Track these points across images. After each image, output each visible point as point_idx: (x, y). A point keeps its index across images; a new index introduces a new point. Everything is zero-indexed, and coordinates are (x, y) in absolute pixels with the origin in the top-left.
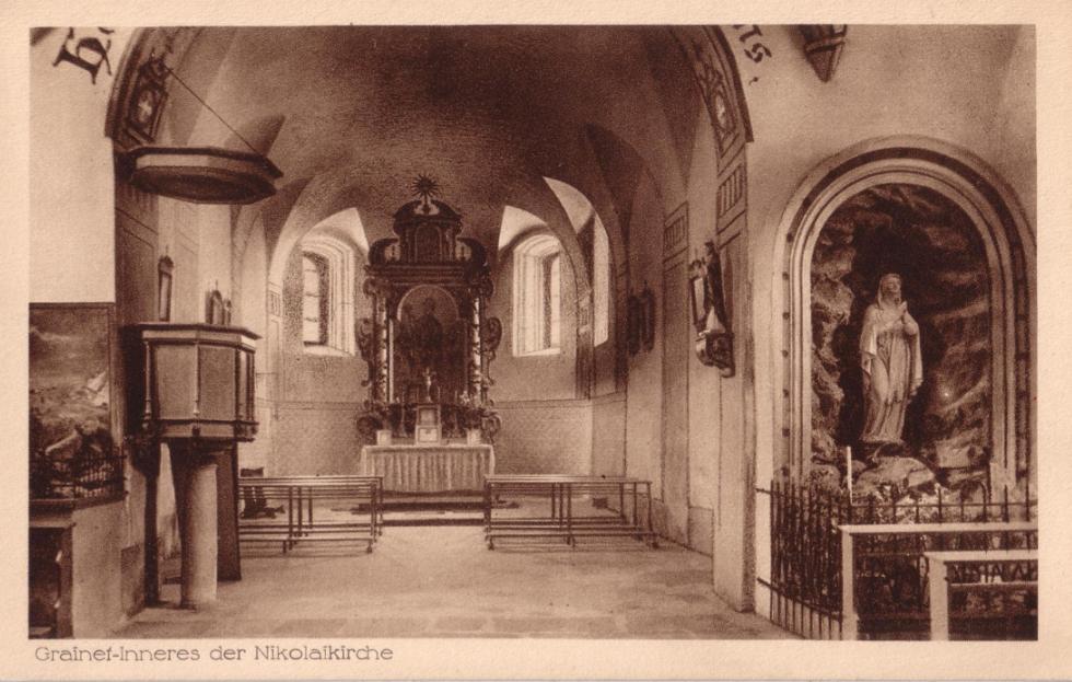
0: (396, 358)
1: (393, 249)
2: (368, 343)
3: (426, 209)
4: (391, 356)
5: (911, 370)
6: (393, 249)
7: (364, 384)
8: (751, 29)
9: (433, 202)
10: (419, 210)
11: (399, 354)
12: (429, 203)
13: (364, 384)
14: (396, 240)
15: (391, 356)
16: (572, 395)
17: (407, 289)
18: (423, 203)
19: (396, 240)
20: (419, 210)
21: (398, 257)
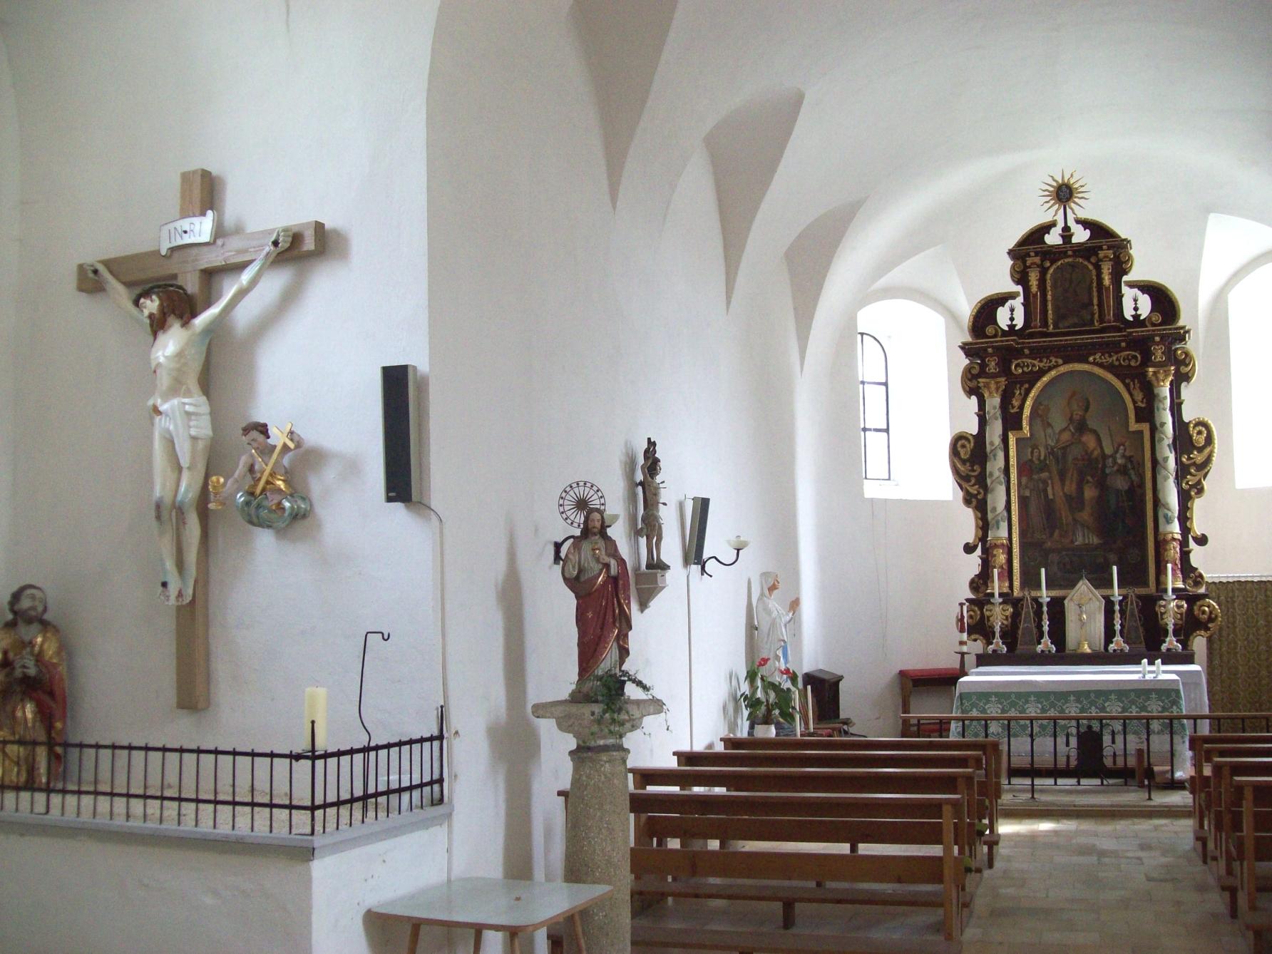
0: (1023, 501)
1: (1012, 310)
2: (969, 458)
3: (1067, 233)
4: (1013, 461)
5: (900, 903)
6: (1012, 310)
7: (969, 549)
8: (1199, 843)
9: (1078, 221)
10: (1053, 238)
11: (1027, 493)
12: (1071, 223)
13: (969, 549)
14: (1012, 296)
15: (1013, 461)
16: (457, 871)
17: (1042, 373)
18: (1061, 225)
19: (1012, 296)
20: (1053, 238)
21: (1019, 322)
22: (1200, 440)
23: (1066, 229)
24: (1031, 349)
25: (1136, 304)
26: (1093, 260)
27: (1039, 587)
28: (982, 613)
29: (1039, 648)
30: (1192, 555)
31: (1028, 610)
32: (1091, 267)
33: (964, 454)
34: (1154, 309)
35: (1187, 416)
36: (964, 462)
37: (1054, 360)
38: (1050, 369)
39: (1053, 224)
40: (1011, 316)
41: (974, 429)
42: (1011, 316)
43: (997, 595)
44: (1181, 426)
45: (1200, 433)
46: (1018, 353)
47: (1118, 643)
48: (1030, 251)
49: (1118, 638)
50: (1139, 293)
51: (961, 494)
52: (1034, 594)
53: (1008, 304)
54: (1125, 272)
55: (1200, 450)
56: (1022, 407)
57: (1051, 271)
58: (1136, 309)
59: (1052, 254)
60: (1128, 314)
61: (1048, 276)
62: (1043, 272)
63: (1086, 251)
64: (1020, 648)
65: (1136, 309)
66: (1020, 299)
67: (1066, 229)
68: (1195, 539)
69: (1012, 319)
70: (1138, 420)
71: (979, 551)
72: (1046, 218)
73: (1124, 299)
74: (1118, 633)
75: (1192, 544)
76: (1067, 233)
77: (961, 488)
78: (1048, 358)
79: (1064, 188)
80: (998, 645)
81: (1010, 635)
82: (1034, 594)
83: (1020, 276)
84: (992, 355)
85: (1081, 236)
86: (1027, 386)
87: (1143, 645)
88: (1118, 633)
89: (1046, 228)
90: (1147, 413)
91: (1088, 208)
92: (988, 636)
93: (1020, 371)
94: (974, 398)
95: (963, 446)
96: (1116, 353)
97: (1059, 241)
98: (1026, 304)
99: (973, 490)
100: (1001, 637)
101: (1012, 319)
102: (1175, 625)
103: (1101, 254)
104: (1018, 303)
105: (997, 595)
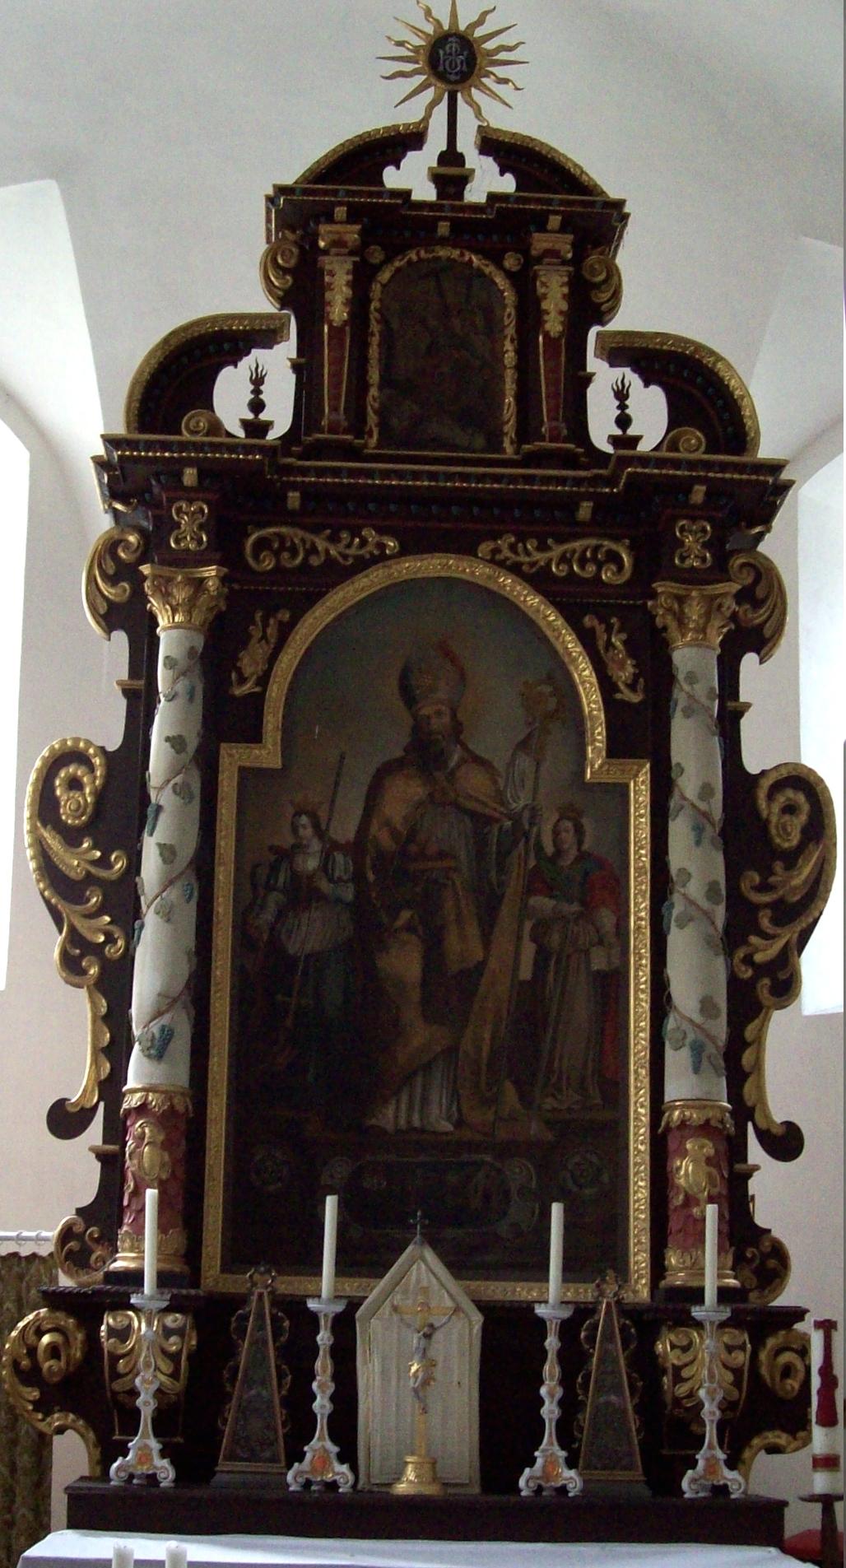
1: (258, 381)
3: (451, 174)
6: (258, 381)
7: (65, 1121)
10: (412, 176)
12: (467, 143)
14: (262, 334)
17: (338, 573)
20: (412, 176)
21: (280, 415)
22: (787, 834)
23: (451, 157)
24: (307, 493)
25: (626, 412)
26: (511, 262)
27: (540, 1270)
28: (93, 1340)
29: (293, 1478)
30: (754, 1186)
31: (256, 1345)
32: (500, 281)
33: (71, 806)
34: (676, 419)
35: (754, 760)
36: (72, 837)
37: (370, 534)
38: (362, 565)
39: (414, 138)
40: (262, 392)
41: (113, 736)
42: (262, 392)
43: (710, 1295)
44: (738, 782)
45: (790, 809)
46: (270, 507)
47: (550, 1467)
48: (337, 210)
49: (549, 1449)
50: (634, 380)
51: (56, 941)
52: (288, 1285)
53: (247, 363)
54: (600, 316)
55: (791, 859)
56: (264, 680)
57: (385, 275)
58: (623, 421)
59: (395, 221)
60: (601, 429)
61: (376, 290)
62: (362, 278)
63: (501, 226)
64: (229, 1472)
65: (623, 421)
66: (287, 349)
67: (451, 157)
68: (765, 1138)
69: (257, 406)
70: (617, 749)
71: (95, 1133)
72: (410, 114)
73: (591, 392)
74: (550, 1430)
75: (755, 1152)
76: (451, 174)
77: (58, 919)
78: (355, 532)
79: (453, 45)
80: (145, 1456)
81: (190, 1424)
82: (288, 1285)
83: (298, 280)
84: (190, 495)
85: (488, 181)
86: (285, 615)
87: (638, 1474)
88: (550, 1430)
89: (397, 144)
90: (641, 731)
91: (520, 105)
92: (110, 1424)
93: (268, 564)
94: (121, 638)
95: (74, 784)
96: (561, 540)
97: (425, 192)
98: (306, 370)
99: (96, 930)
100: (159, 1430)
101: (257, 406)
102: (160, 1393)
103: (540, 242)
104: (277, 363)
105: (710, 1295)
